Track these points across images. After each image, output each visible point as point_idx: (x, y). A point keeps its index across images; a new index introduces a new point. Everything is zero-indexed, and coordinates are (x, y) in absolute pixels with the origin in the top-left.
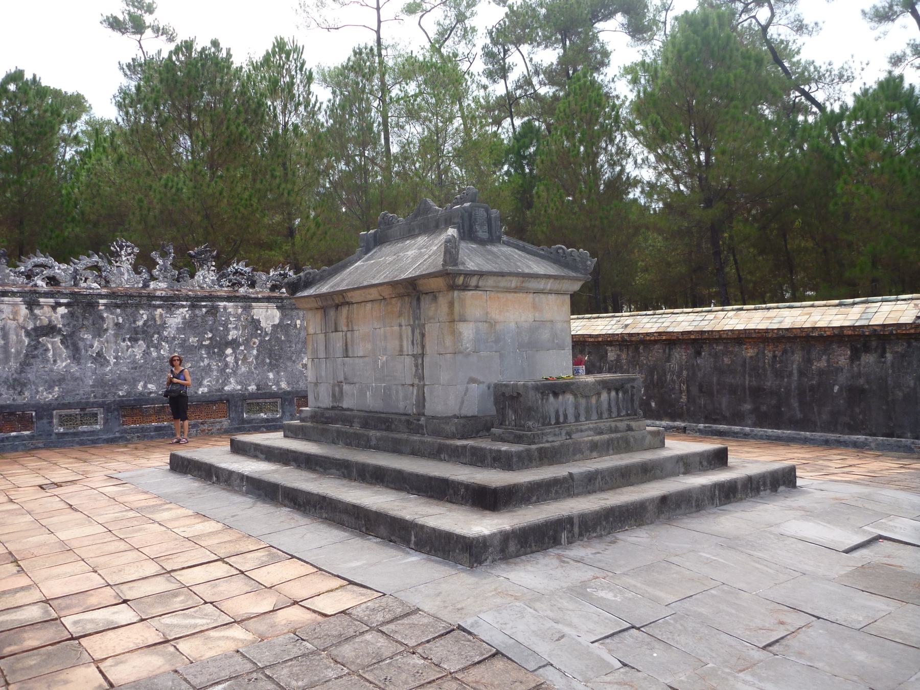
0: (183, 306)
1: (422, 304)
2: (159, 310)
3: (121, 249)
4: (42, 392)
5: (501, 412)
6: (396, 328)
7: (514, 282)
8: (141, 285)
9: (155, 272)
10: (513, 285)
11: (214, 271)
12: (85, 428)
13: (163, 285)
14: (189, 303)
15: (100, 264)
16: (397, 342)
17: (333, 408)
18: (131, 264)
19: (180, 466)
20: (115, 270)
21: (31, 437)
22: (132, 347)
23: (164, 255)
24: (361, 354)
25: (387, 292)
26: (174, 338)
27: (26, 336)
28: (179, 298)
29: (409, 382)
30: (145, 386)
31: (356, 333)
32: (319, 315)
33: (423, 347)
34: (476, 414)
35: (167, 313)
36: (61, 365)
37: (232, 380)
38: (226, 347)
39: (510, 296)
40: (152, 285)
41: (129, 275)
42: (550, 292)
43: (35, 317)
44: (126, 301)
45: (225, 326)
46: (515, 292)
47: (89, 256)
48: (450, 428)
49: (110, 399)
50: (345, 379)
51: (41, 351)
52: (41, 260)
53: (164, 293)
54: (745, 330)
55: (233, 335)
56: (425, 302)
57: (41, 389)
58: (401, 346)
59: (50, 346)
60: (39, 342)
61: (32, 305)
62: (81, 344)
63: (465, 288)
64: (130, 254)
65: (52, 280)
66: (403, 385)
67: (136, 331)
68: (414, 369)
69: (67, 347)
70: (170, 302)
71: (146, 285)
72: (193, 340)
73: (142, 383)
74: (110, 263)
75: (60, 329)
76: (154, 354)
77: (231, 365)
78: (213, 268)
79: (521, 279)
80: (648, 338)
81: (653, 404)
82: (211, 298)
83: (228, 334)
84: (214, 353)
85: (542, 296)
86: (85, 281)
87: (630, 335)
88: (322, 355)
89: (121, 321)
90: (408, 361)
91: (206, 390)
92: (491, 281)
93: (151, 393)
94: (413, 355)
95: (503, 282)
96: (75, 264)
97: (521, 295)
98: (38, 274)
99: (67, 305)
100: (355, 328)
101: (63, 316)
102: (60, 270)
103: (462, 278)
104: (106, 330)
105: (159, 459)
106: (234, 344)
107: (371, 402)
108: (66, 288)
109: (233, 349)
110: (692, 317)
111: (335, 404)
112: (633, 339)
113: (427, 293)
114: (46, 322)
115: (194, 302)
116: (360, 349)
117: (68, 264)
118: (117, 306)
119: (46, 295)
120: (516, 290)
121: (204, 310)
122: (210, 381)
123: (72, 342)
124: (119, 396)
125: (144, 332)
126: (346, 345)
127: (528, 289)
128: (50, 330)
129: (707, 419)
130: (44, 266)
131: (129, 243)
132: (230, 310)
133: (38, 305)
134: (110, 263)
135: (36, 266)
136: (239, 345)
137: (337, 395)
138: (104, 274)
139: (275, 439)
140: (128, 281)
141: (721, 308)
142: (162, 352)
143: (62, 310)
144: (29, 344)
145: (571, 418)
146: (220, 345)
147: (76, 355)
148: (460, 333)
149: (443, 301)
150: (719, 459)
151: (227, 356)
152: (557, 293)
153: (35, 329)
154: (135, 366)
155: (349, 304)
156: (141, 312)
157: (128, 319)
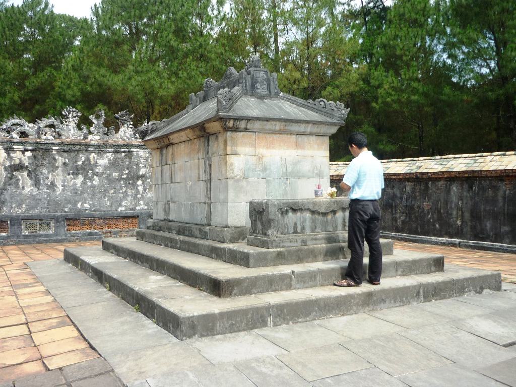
0: (109, 152)
1: (210, 142)
2: (93, 154)
3: (69, 114)
4: (15, 208)
5: (254, 223)
6: (196, 161)
7: (278, 126)
8: (82, 138)
9: (92, 129)
10: (277, 128)
11: (131, 128)
12: (43, 232)
13: (98, 138)
14: (113, 150)
15: (55, 124)
16: (197, 171)
17: (165, 220)
18: (75, 123)
19: (71, 259)
20: (65, 127)
21: (8, 237)
22: (74, 179)
23: (98, 117)
24: (179, 181)
25: (190, 134)
26: (102, 173)
27: (5, 171)
28: (106, 146)
29: (203, 201)
30: (82, 205)
31: (176, 165)
32: (158, 152)
33: (210, 174)
34: (244, 225)
35: (98, 156)
36: (28, 190)
37: (142, 202)
38: (138, 179)
39: (276, 137)
40: (90, 137)
41: (74, 130)
42: (311, 134)
43: (11, 158)
44: (71, 149)
45: (137, 165)
46: (281, 134)
47: (48, 119)
48: (227, 233)
49: (58, 214)
50: (171, 199)
51: (14, 180)
52: (16, 121)
53: (96, 143)
54: (512, 170)
55: (142, 171)
56: (212, 139)
57: (14, 205)
58: (199, 175)
59: (20, 178)
60: (13, 175)
61: (9, 150)
62: (41, 177)
63: (236, 129)
64: (75, 117)
65: (23, 134)
66: (200, 203)
67: (77, 168)
68: (205, 191)
69: (31, 179)
70: (100, 149)
71: (85, 138)
72: (115, 175)
73: (80, 204)
74: (62, 123)
75: (27, 167)
76: (89, 184)
77: (141, 192)
78: (131, 126)
79: (283, 123)
80: (434, 176)
81: (437, 226)
82: (127, 146)
83: (139, 171)
84: (129, 184)
85: (304, 137)
86: (45, 135)
87: (422, 174)
88: (160, 182)
89: (67, 161)
90: (202, 184)
91: (123, 209)
92: (257, 125)
93: (87, 210)
94: (205, 181)
95: (269, 126)
96: (39, 123)
97: (286, 135)
98: (14, 130)
99: (32, 150)
100: (176, 162)
101: (29, 158)
102: (29, 127)
103: (232, 122)
104: (57, 167)
105: (56, 253)
106: (143, 177)
107: (185, 217)
108: (32, 139)
109: (143, 181)
110: (468, 160)
111: (166, 218)
112: (424, 176)
113: (212, 135)
114: (18, 161)
115: (117, 149)
116: (179, 177)
117: (34, 124)
118: (65, 151)
119: (18, 143)
120: (281, 132)
121: (123, 154)
122: (126, 203)
123: (33, 174)
124: (65, 212)
125: (83, 169)
126: (171, 175)
127: (290, 131)
128: (20, 167)
129: (476, 237)
130: (17, 124)
131: (74, 109)
132: (141, 154)
133: (13, 150)
134: (62, 123)
135: (13, 125)
136: (147, 178)
137: (167, 211)
138: (57, 130)
139: (129, 242)
140: (73, 135)
141: (489, 154)
142: (94, 182)
143: (29, 154)
144: (6, 176)
145: (308, 229)
146: (134, 178)
147: (37, 184)
148: (232, 164)
149: (221, 139)
150: (439, 264)
151: (138, 186)
152: (318, 135)
153: (11, 166)
154: (75, 192)
155: (173, 144)
156: (81, 155)
157: (72, 161)
